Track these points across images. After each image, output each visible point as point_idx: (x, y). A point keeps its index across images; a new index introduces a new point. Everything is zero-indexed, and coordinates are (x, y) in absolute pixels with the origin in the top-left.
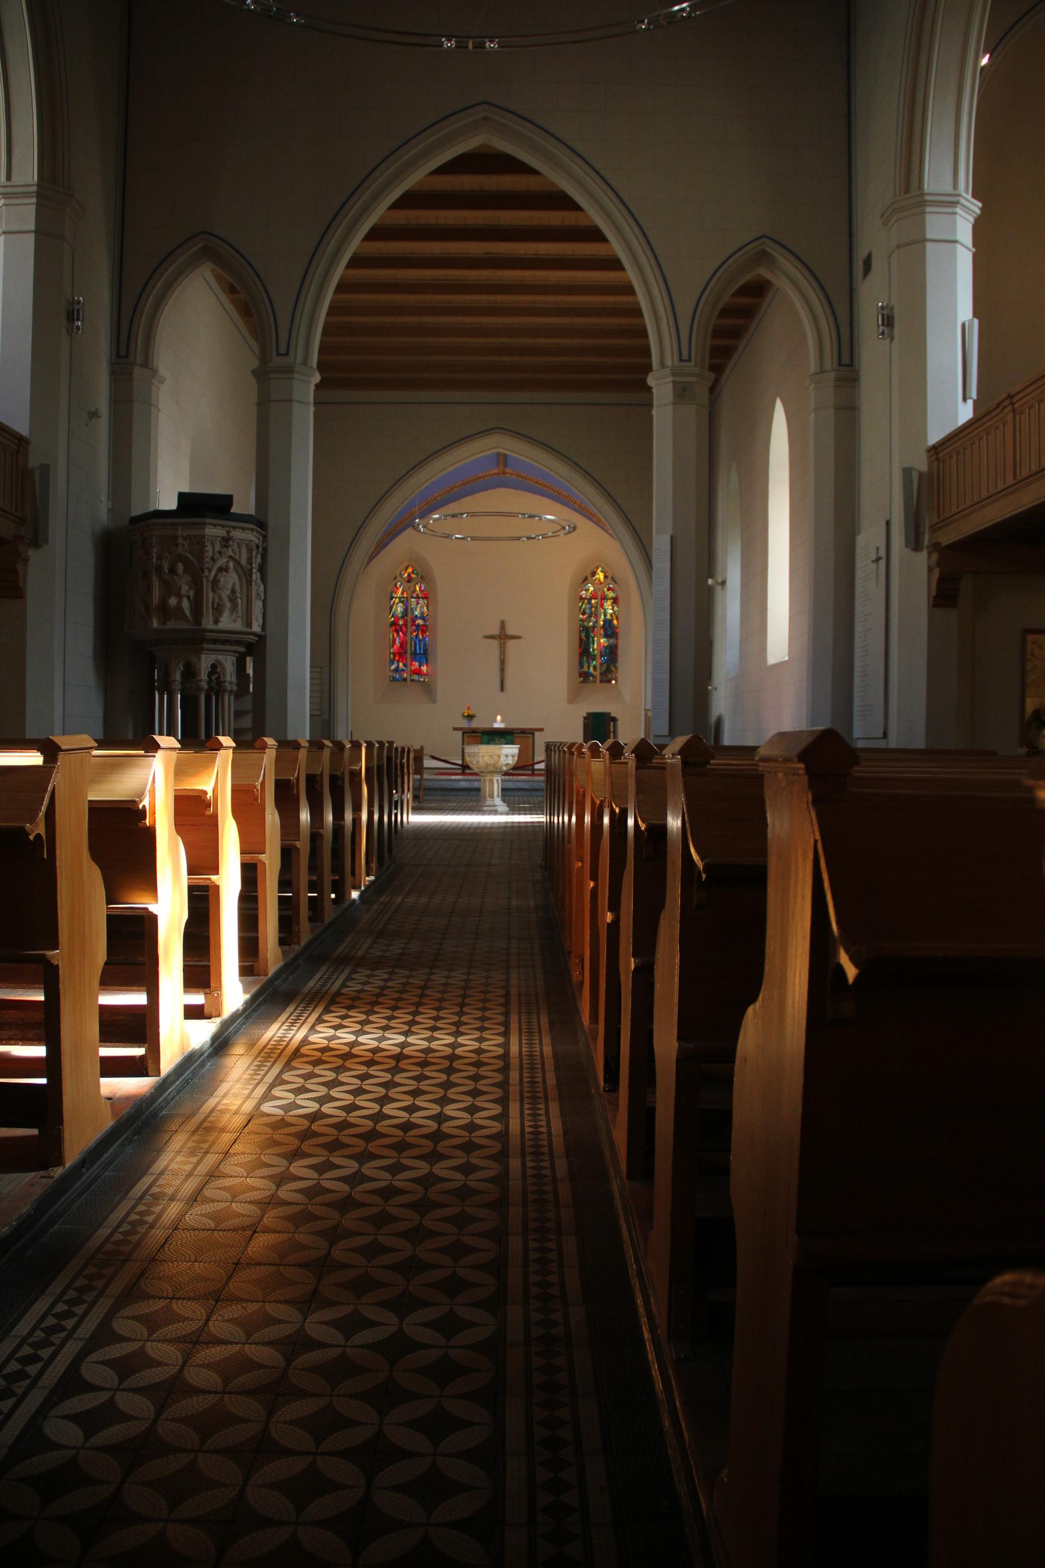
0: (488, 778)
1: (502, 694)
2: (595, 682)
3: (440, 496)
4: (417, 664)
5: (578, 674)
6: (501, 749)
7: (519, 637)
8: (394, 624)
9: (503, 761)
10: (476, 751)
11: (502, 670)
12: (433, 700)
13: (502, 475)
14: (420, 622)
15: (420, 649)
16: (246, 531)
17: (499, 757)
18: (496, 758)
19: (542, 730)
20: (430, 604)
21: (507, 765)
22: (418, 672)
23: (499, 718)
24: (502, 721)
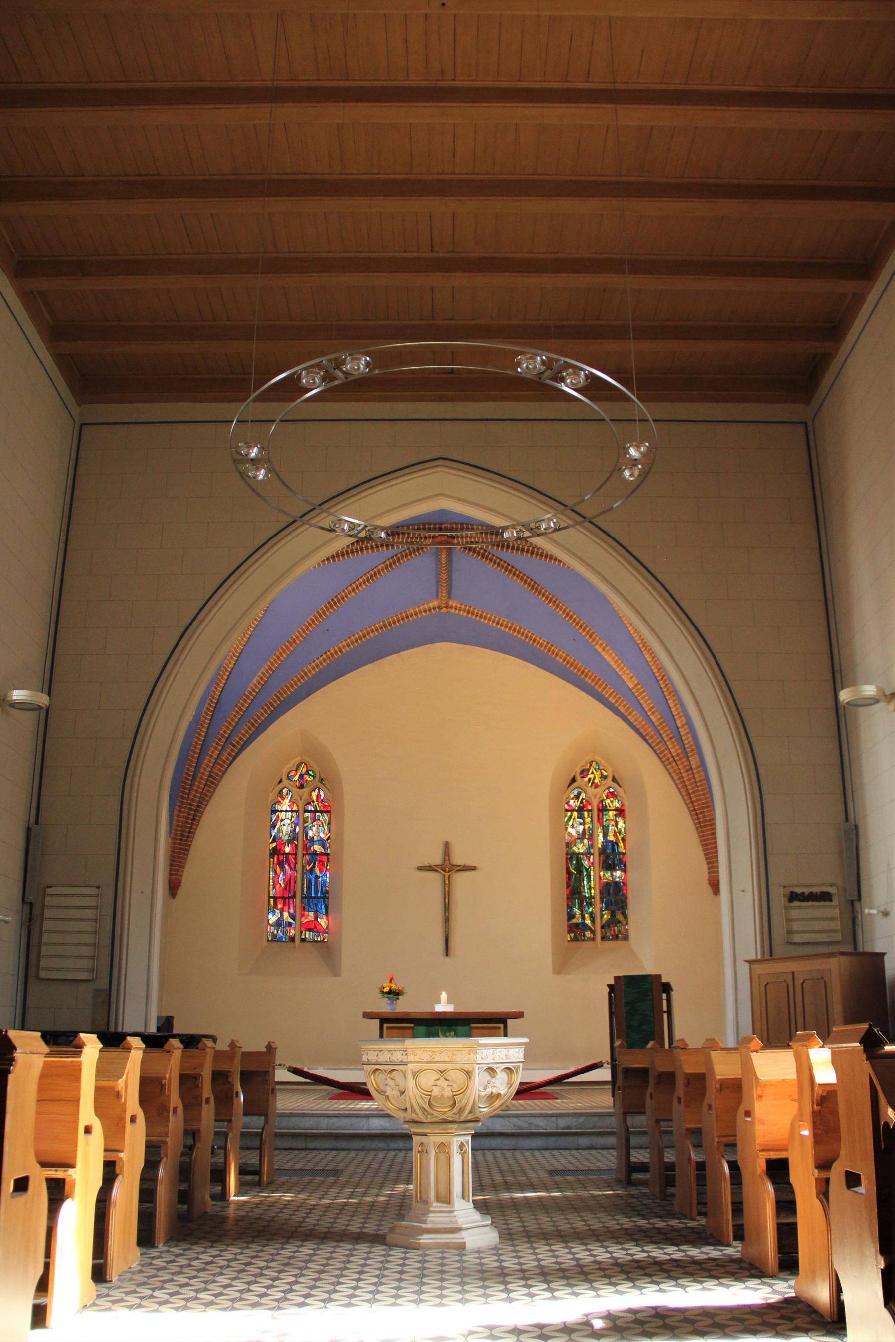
1: (447, 959)
2: (594, 939)
3: (348, 646)
4: (312, 914)
5: (566, 928)
7: (474, 868)
8: (276, 852)
9: (480, 1085)
10: (398, 1056)
11: (447, 920)
12: (334, 968)
13: (444, 610)
14: (317, 848)
15: (316, 892)
16: (425, 1125)
17: (469, 1074)
18: (458, 1077)
19: (519, 1015)
20: (332, 822)
21: (493, 1097)
22: (313, 927)
23: (444, 996)
24: (449, 1002)
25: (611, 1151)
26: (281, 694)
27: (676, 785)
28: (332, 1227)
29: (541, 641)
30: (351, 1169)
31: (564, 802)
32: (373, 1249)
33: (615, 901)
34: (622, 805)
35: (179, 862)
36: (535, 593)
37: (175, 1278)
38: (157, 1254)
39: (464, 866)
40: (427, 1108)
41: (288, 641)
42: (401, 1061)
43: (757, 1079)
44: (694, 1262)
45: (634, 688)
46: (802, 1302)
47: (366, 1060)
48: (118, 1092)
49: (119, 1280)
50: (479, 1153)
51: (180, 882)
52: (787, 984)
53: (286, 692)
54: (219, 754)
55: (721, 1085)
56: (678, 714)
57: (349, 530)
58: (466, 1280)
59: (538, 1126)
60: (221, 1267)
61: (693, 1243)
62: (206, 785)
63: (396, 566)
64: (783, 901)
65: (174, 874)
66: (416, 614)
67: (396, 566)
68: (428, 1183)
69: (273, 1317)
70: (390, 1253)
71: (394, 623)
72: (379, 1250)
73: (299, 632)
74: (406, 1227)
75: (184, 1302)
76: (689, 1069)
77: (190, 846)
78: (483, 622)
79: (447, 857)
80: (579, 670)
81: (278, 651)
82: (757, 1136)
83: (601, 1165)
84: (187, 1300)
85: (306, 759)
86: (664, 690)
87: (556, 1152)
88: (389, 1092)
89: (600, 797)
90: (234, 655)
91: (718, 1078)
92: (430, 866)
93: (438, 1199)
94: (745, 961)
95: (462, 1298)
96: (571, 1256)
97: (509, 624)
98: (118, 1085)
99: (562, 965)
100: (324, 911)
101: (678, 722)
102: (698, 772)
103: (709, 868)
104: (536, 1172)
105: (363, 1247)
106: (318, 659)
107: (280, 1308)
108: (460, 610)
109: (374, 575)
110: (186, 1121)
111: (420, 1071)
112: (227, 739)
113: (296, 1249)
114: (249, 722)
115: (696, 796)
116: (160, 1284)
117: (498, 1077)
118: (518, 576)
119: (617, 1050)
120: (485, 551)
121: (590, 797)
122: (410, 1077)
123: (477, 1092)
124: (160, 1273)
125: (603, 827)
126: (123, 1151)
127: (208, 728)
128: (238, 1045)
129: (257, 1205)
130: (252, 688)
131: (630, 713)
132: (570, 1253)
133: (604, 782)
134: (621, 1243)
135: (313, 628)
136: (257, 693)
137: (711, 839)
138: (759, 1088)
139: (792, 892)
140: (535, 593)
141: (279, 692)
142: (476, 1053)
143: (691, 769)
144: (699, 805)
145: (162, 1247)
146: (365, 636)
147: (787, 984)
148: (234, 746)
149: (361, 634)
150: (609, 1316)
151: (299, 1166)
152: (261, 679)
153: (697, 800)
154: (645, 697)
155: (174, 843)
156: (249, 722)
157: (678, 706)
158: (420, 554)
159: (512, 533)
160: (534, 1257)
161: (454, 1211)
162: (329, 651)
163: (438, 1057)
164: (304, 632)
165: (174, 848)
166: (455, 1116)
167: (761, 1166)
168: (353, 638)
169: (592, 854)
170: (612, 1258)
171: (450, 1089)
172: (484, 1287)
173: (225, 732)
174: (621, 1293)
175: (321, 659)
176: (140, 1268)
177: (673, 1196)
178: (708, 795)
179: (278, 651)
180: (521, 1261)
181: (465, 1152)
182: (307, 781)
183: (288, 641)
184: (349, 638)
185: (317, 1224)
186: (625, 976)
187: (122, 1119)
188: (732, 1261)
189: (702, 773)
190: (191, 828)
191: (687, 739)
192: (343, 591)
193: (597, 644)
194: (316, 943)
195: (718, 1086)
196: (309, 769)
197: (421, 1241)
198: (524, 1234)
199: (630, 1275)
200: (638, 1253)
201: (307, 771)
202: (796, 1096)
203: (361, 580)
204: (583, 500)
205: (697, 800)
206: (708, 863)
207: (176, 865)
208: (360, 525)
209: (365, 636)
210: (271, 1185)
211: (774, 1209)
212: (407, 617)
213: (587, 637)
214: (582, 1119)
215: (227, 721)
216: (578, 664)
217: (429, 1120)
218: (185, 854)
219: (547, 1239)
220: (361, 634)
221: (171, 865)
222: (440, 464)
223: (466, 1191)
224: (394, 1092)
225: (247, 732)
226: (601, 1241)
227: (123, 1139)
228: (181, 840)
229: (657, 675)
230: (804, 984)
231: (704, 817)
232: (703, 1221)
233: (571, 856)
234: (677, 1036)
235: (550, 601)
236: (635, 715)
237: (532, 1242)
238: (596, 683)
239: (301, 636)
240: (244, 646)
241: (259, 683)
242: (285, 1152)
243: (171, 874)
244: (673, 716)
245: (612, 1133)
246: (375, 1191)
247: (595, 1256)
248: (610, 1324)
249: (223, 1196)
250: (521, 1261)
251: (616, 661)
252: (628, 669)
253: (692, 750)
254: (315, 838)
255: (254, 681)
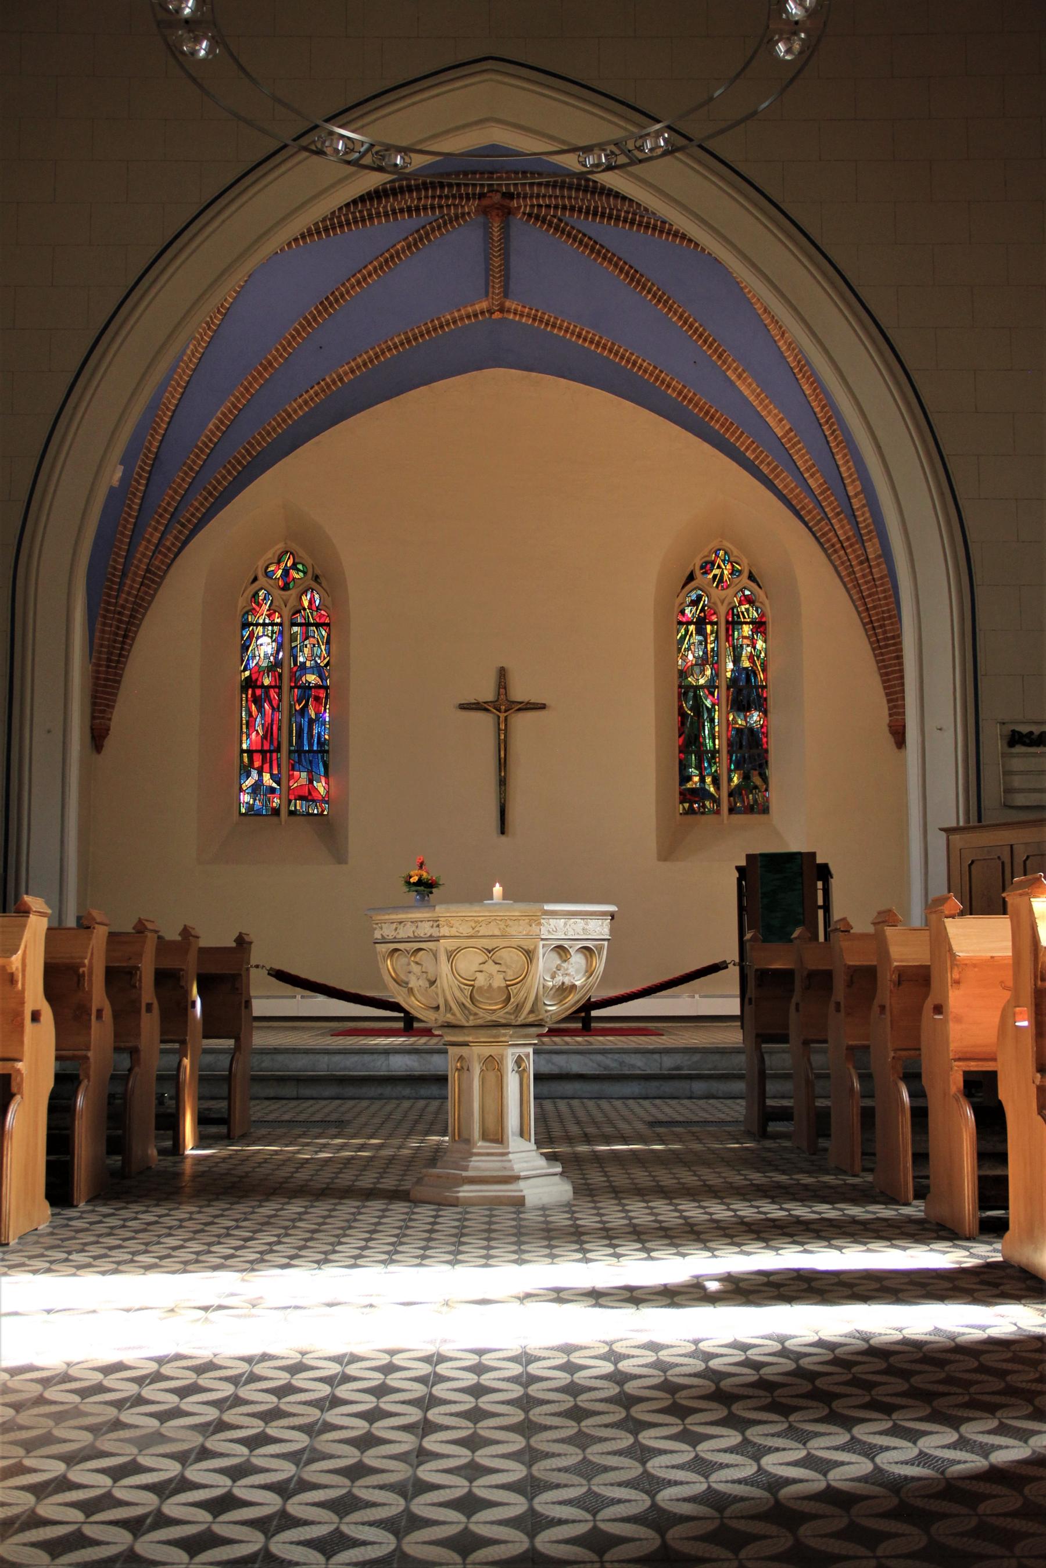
0: (478, 1052)
1: (503, 838)
3: (352, 371)
4: (304, 775)
6: (534, 920)
7: (542, 707)
8: (249, 684)
10: (426, 929)
11: (503, 782)
12: (340, 857)
13: (497, 315)
14: (312, 678)
15: (311, 744)
16: (466, 1031)
17: (529, 955)
21: (564, 990)
22: (309, 796)
25: (738, 1101)
26: (252, 446)
27: (845, 584)
28: (332, 1183)
29: (645, 364)
30: (362, 1119)
31: (676, 610)
32: (391, 1207)
33: (749, 757)
34: (762, 615)
35: (105, 699)
36: (636, 287)
37: (101, 1240)
38: (78, 1214)
39: (528, 703)
40: (468, 1003)
41: (261, 364)
42: (431, 936)
43: (953, 955)
44: (854, 1221)
45: (784, 436)
46: (1012, 1266)
47: (379, 937)
48: (12, 975)
49: (19, 1243)
50: (548, 1105)
51: (108, 729)
52: (1003, 863)
53: (259, 444)
54: (160, 539)
55: (899, 975)
56: (851, 475)
57: (346, 153)
58: (524, 1239)
59: (633, 1066)
60: (170, 1228)
61: (855, 1202)
62: (142, 584)
63: (423, 244)
64: (1000, 745)
65: (99, 718)
66: (455, 322)
67: (423, 244)
68: (471, 1114)
69: (243, 1280)
70: (415, 1210)
71: (422, 336)
72: (399, 1208)
73: (277, 350)
74: (439, 1177)
75: (115, 1266)
76: (853, 960)
77: (121, 676)
78: (557, 335)
79: (502, 691)
80: (701, 410)
81: (246, 379)
82: (951, 1039)
83: (722, 1116)
84: (119, 1263)
85: (294, 546)
86: (830, 439)
87: (658, 1102)
88: (413, 983)
89: (730, 603)
90: (179, 385)
91: (896, 964)
92: (478, 703)
93: (485, 1137)
94: (941, 830)
95: (528, 1363)
96: (677, 1214)
97: (597, 338)
98: (11, 963)
99: (669, 850)
100: (322, 769)
101: (849, 488)
102: (878, 565)
103: (890, 709)
104: (629, 1123)
105: (378, 1205)
106: (307, 392)
107: (253, 1270)
108: (522, 315)
109: (389, 260)
110: (117, 1035)
111: (459, 950)
112: (173, 515)
113: (280, 1206)
114: (205, 489)
115: (873, 601)
116: (80, 1247)
117: (572, 960)
118: (610, 261)
119: (748, 946)
120: (560, 220)
121: (715, 603)
122: (443, 958)
123: (542, 980)
124: (79, 1235)
125: (734, 648)
126: (21, 1060)
127: (143, 498)
128: (193, 932)
129: (224, 1160)
130: (207, 436)
131: (777, 476)
132: (676, 1210)
133: (736, 581)
134: (750, 1201)
135: (298, 343)
136: (216, 444)
137: (895, 665)
138: (956, 970)
139: (1013, 731)
140: (636, 287)
141: (249, 443)
142: (540, 924)
143: (867, 560)
144: (877, 614)
145: (82, 1205)
146: (377, 357)
147: (1003, 863)
148: (183, 525)
149: (371, 353)
150: (728, 1279)
151: (286, 1117)
152: (222, 422)
153: (875, 608)
154: (800, 450)
155: (98, 672)
156: (205, 489)
157: (851, 464)
158: (459, 225)
159: (600, 157)
160: (624, 1215)
161: (509, 1153)
162: (324, 380)
163: (483, 931)
164: (285, 349)
165: (98, 678)
166: (508, 1016)
167: (957, 1081)
168: (359, 360)
169: (717, 687)
170: (736, 1216)
171: (501, 976)
172: (550, 1247)
173: (169, 504)
174: (749, 1254)
175: (312, 392)
176: (51, 1230)
177: (826, 1150)
178: (893, 599)
179: (246, 379)
180: (604, 1218)
181: (524, 1070)
182: (294, 579)
183: (261, 364)
184: (354, 359)
185: (311, 1180)
186: (761, 855)
187: (18, 1015)
188: (910, 1220)
189: (884, 566)
190: (122, 649)
191: (863, 514)
192: (343, 285)
193: (729, 368)
194: (311, 818)
195: (895, 977)
196: (297, 560)
197: (461, 1194)
198: (610, 1190)
199: (762, 1235)
200: (774, 1211)
201: (294, 565)
202: (1010, 983)
203: (370, 267)
204: (711, 99)
205: (875, 608)
206: (889, 701)
207: (101, 704)
208: (363, 143)
209: (377, 357)
210: (245, 1138)
211: (975, 1138)
212: (442, 327)
213: (715, 358)
214: (696, 1057)
215: (171, 488)
216: (700, 400)
217: (471, 1023)
218: (113, 688)
219: (643, 1195)
220: (371, 353)
221: (94, 704)
222: (489, 67)
223: (525, 1112)
224: (421, 982)
225: (202, 504)
226: (721, 1198)
227: (22, 1043)
228: (108, 667)
229: (819, 416)
230: (1028, 862)
231: (885, 632)
232: (870, 1178)
233: (686, 691)
234: (836, 915)
235: (659, 301)
236: (784, 479)
237: (620, 1199)
238: (727, 430)
239: (281, 355)
240: (194, 370)
241: (218, 428)
242: (267, 1103)
243: (93, 718)
244: (842, 479)
245: (740, 1077)
246: (396, 1142)
247: (711, 1214)
248: (730, 1287)
249: (177, 1147)
250: (604, 1218)
251: (759, 395)
252: (775, 408)
253: (870, 532)
254: (308, 664)
255: (211, 426)
